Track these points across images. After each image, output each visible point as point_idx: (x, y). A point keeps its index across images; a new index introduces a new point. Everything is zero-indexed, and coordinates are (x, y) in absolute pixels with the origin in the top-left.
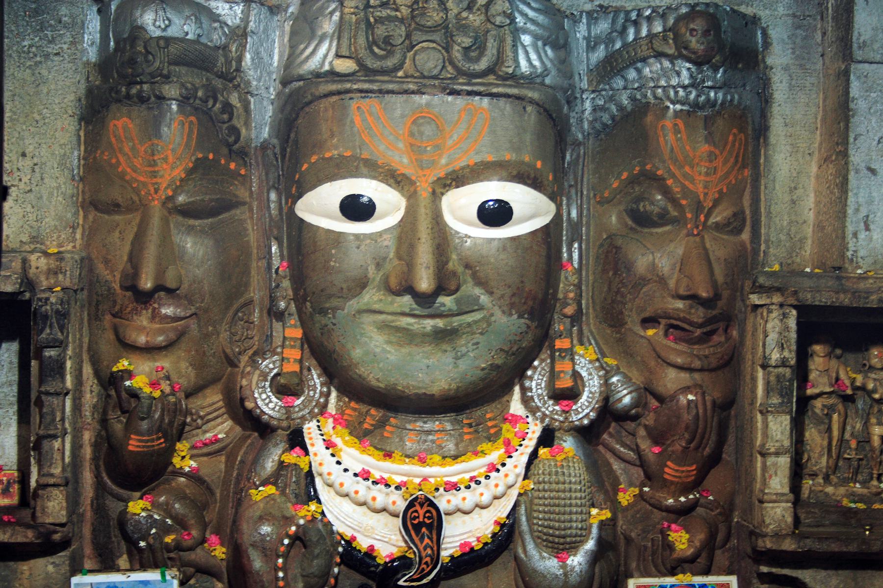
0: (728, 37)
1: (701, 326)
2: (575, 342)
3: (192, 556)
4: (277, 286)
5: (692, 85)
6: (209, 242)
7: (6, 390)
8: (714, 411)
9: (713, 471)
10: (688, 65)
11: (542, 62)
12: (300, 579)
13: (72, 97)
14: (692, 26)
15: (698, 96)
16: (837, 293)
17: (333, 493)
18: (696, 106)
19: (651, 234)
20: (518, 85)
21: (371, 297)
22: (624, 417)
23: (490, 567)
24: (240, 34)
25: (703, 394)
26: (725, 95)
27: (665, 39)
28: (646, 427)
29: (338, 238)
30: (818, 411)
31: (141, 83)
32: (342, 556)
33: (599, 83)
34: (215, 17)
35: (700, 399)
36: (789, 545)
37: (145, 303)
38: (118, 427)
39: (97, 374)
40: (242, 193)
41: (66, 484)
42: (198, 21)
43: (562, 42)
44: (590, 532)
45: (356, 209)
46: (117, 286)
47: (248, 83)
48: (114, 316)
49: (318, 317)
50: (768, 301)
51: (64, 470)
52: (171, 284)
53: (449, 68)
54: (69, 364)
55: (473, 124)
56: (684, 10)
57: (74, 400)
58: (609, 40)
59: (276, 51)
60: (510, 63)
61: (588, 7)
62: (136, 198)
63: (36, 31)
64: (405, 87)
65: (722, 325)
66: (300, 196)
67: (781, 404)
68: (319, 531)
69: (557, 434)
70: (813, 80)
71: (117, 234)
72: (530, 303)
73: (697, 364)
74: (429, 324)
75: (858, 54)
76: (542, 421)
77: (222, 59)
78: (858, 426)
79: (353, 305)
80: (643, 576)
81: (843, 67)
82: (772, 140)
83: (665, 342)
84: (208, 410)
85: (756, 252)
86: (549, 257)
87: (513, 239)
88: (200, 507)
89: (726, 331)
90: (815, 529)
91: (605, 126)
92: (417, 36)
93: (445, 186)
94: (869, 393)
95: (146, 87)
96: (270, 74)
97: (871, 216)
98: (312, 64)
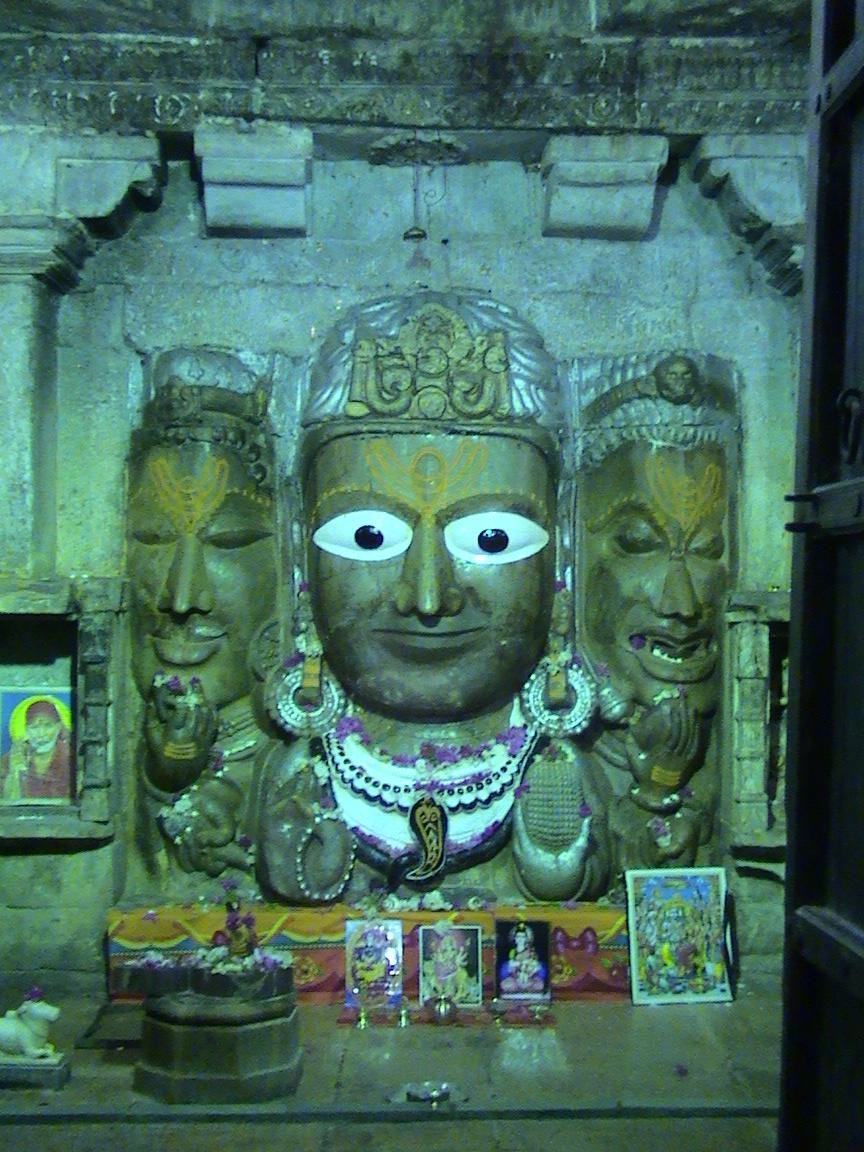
1: (683, 642)
3: (223, 851)
22: (615, 726)
24: (265, 384)
29: (352, 565)
31: (177, 426)
34: (243, 367)
38: (157, 735)
39: (140, 687)
40: (268, 525)
41: (109, 786)
44: (580, 831)
45: (368, 538)
53: (450, 411)
64: (411, 428)
73: (681, 677)
84: (239, 719)
85: (734, 575)
95: (181, 431)
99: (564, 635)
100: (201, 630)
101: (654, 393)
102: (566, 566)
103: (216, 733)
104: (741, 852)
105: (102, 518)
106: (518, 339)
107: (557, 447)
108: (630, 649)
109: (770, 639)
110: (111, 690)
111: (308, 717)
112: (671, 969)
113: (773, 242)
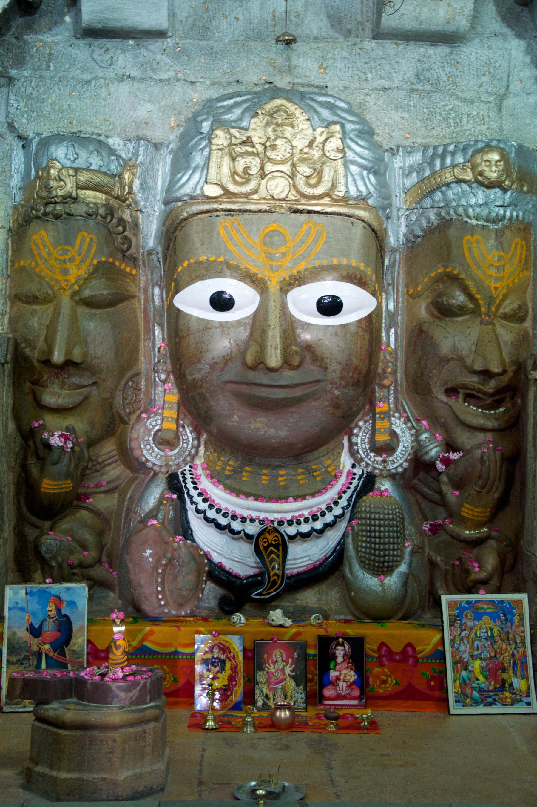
1: (492, 395)
29: (207, 325)
34: (112, 152)
38: (34, 471)
45: (222, 303)
47: (136, 203)
48: (33, 383)
58: (419, 169)
62: (50, 292)
65: (509, 394)
66: (177, 291)
87: (344, 326)
98: (187, 190)
111: (166, 456)
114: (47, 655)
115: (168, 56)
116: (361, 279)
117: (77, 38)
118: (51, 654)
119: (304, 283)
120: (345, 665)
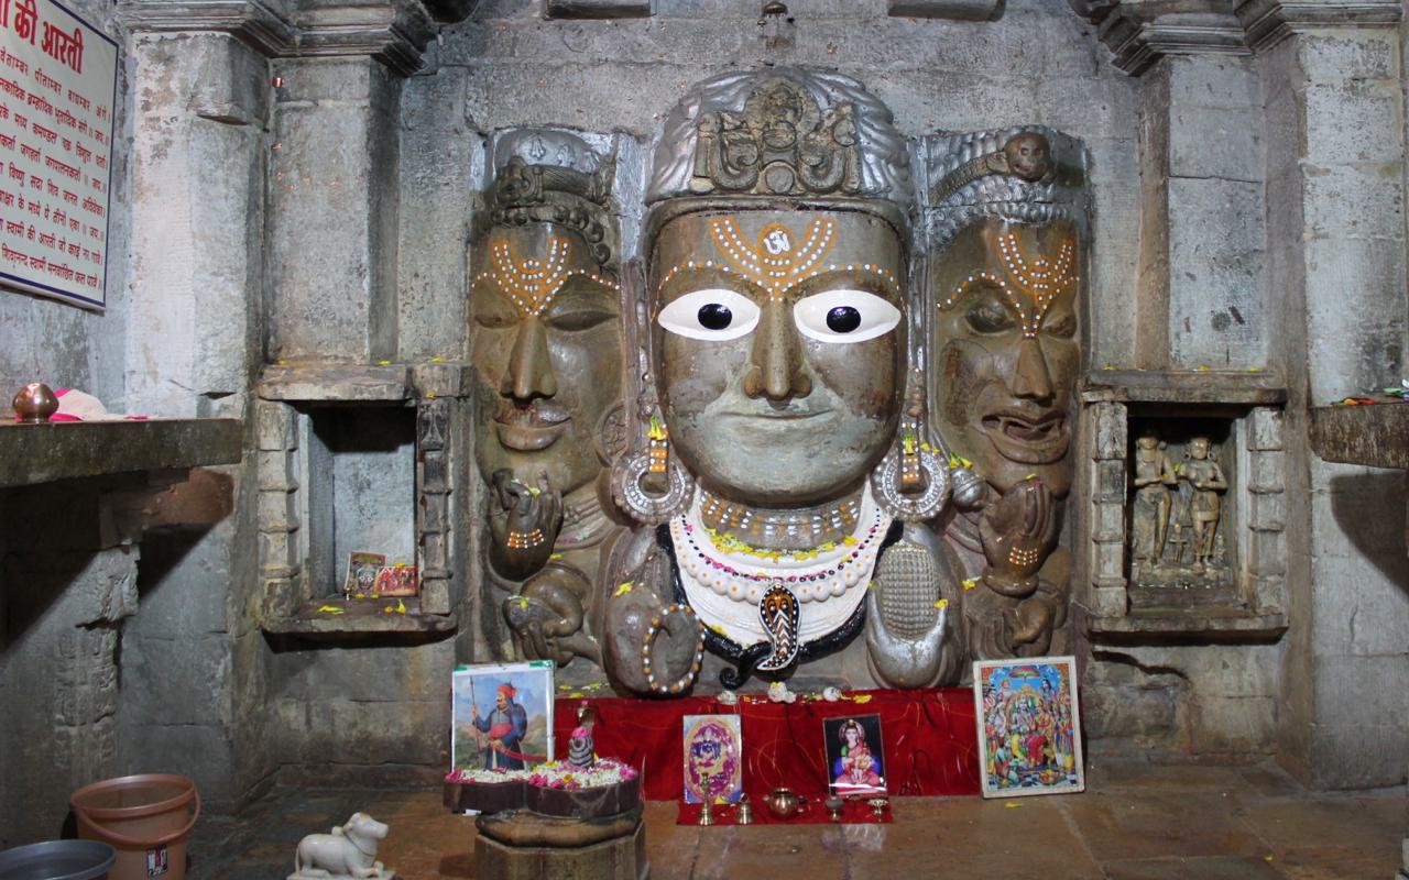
0: (1056, 156)
1: (1038, 423)
2: (921, 439)
3: (569, 641)
4: (644, 391)
5: (1025, 200)
6: (582, 352)
7: (403, 489)
8: (1051, 501)
9: (1051, 557)
10: (1020, 182)
11: (885, 179)
12: (665, 666)
13: (459, 223)
14: (1023, 145)
15: (1031, 210)
16: (1164, 389)
17: (696, 583)
18: (1029, 219)
19: (990, 338)
20: (863, 200)
21: (731, 399)
22: (966, 508)
23: (845, 651)
24: (610, 162)
25: (1041, 486)
26: (1054, 209)
27: (999, 158)
28: (988, 518)
29: (697, 345)
30: (1146, 499)
31: (518, 207)
32: (704, 643)
33: (938, 201)
34: (587, 147)
35: (1038, 491)
36: (1123, 627)
37: (524, 409)
38: (500, 523)
39: (483, 474)
40: (612, 307)
41: (450, 576)
42: (571, 150)
43: (903, 161)
44: (937, 619)
45: (714, 318)
46: (497, 393)
47: (618, 206)
48: (497, 420)
49: (680, 420)
50: (1100, 398)
51: (447, 563)
52: (547, 391)
53: (799, 185)
54: (451, 466)
55: (825, 238)
56: (1015, 132)
57: (458, 499)
58: (947, 161)
59: (643, 176)
60: (856, 179)
61: (928, 132)
62: (515, 313)
63: (427, 164)
64: (758, 203)
65: (1056, 421)
66: (663, 307)
67: (1114, 494)
68: (682, 620)
69: (906, 526)
70: (1134, 196)
71: (498, 346)
72: (878, 404)
73: (1035, 458)
74: (782, 425)
75: (1175, 170)
76: (892, 513)
77: (592, 185)
78: (1182, 512)
79: (714, 408)
80: (990, 658)
81: (1161, 182)
82: (1098, 250)
83: (1006, 438)
84: (584, 506)
85: (1086, 354)
86: (895, 360)
87: (861, 344)
88: (577, 596)
89: (1060, 427)
90: (1145, 610)
91: (946, 239)
92: (768, 157)
93: (796, 295)
94: (1192, 482)
95: (522, 210)
96: (637, 197)
97: (1192, 319)
98: (672, 185)
99: (918, 417)
100: (546, 415)
101: (1005, 169)
102: (918, 346)
103: (562, 520)
104: (1095, 637)
105: (443, 302)
106: (866, 114)
107: (908, 223)
108: (984, 431)
109: (1129, 419)
110: (450, 478)
111: (654, 504)
112: (1021, 760)
113: (1122, 20)
114: (498, 752)
115: (651, 37)
116: (881, 287)
117: (546, 20)
118: (503, 750)
119: (813, 294)
120: (859, 749)
